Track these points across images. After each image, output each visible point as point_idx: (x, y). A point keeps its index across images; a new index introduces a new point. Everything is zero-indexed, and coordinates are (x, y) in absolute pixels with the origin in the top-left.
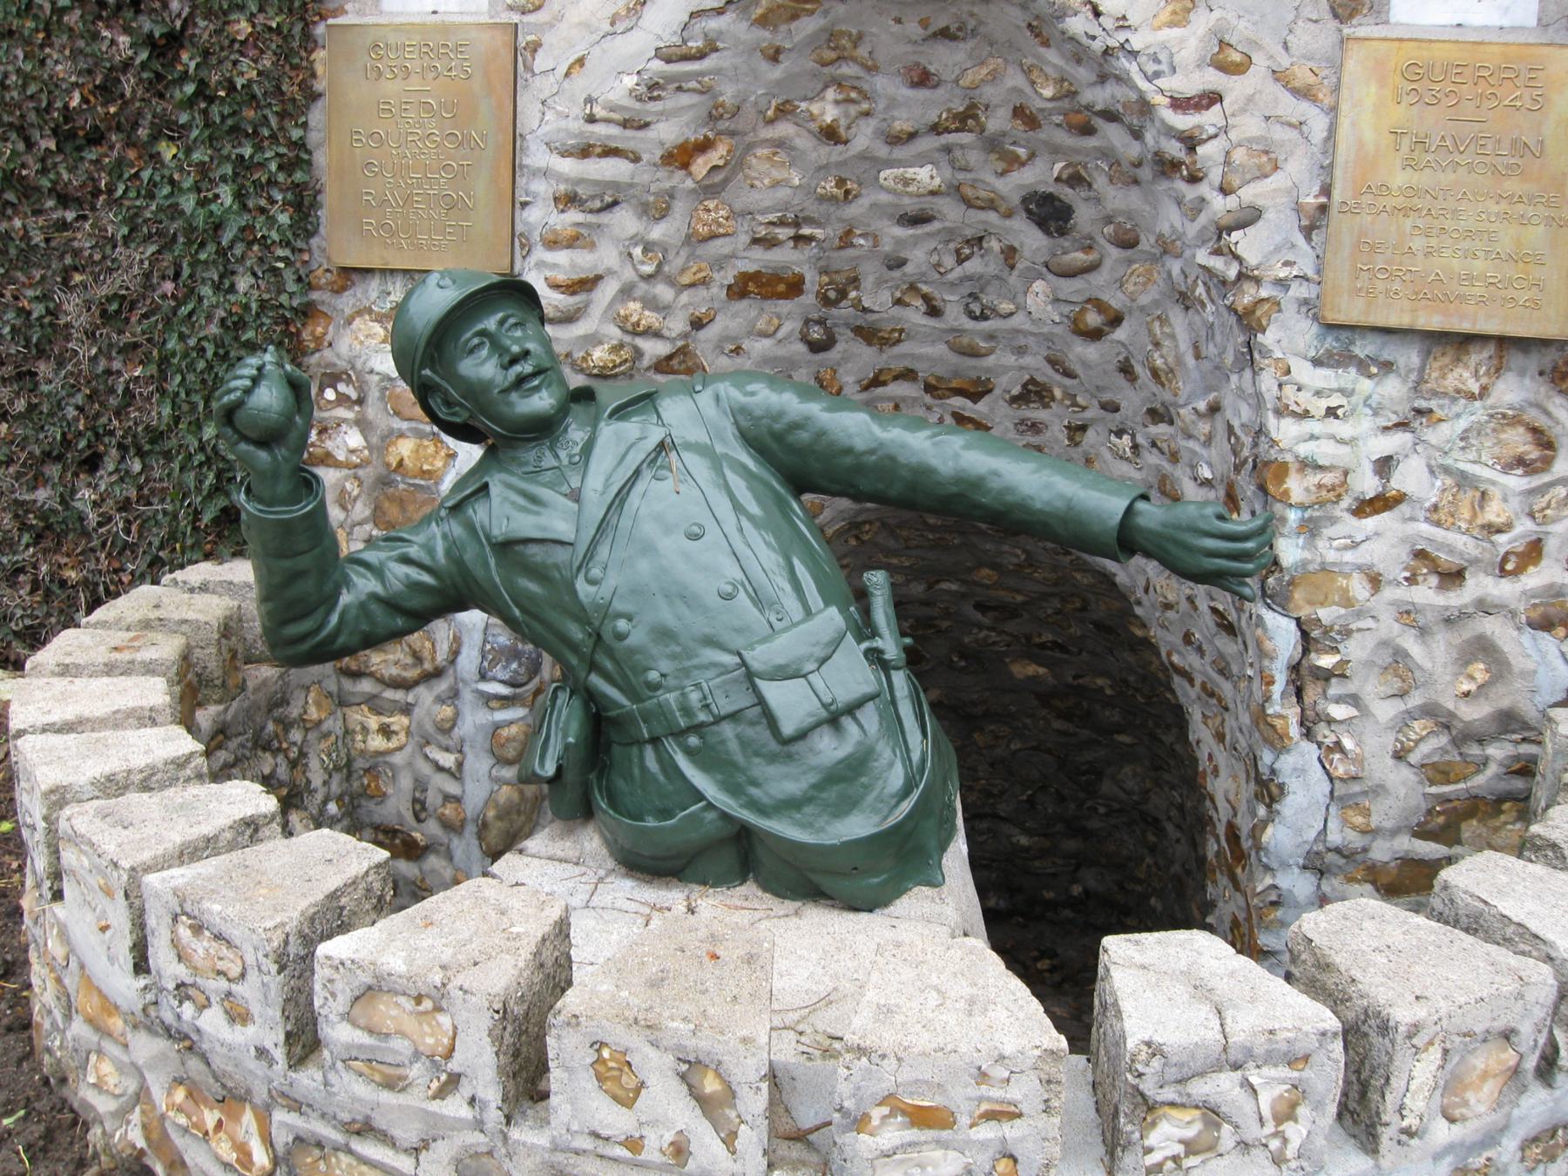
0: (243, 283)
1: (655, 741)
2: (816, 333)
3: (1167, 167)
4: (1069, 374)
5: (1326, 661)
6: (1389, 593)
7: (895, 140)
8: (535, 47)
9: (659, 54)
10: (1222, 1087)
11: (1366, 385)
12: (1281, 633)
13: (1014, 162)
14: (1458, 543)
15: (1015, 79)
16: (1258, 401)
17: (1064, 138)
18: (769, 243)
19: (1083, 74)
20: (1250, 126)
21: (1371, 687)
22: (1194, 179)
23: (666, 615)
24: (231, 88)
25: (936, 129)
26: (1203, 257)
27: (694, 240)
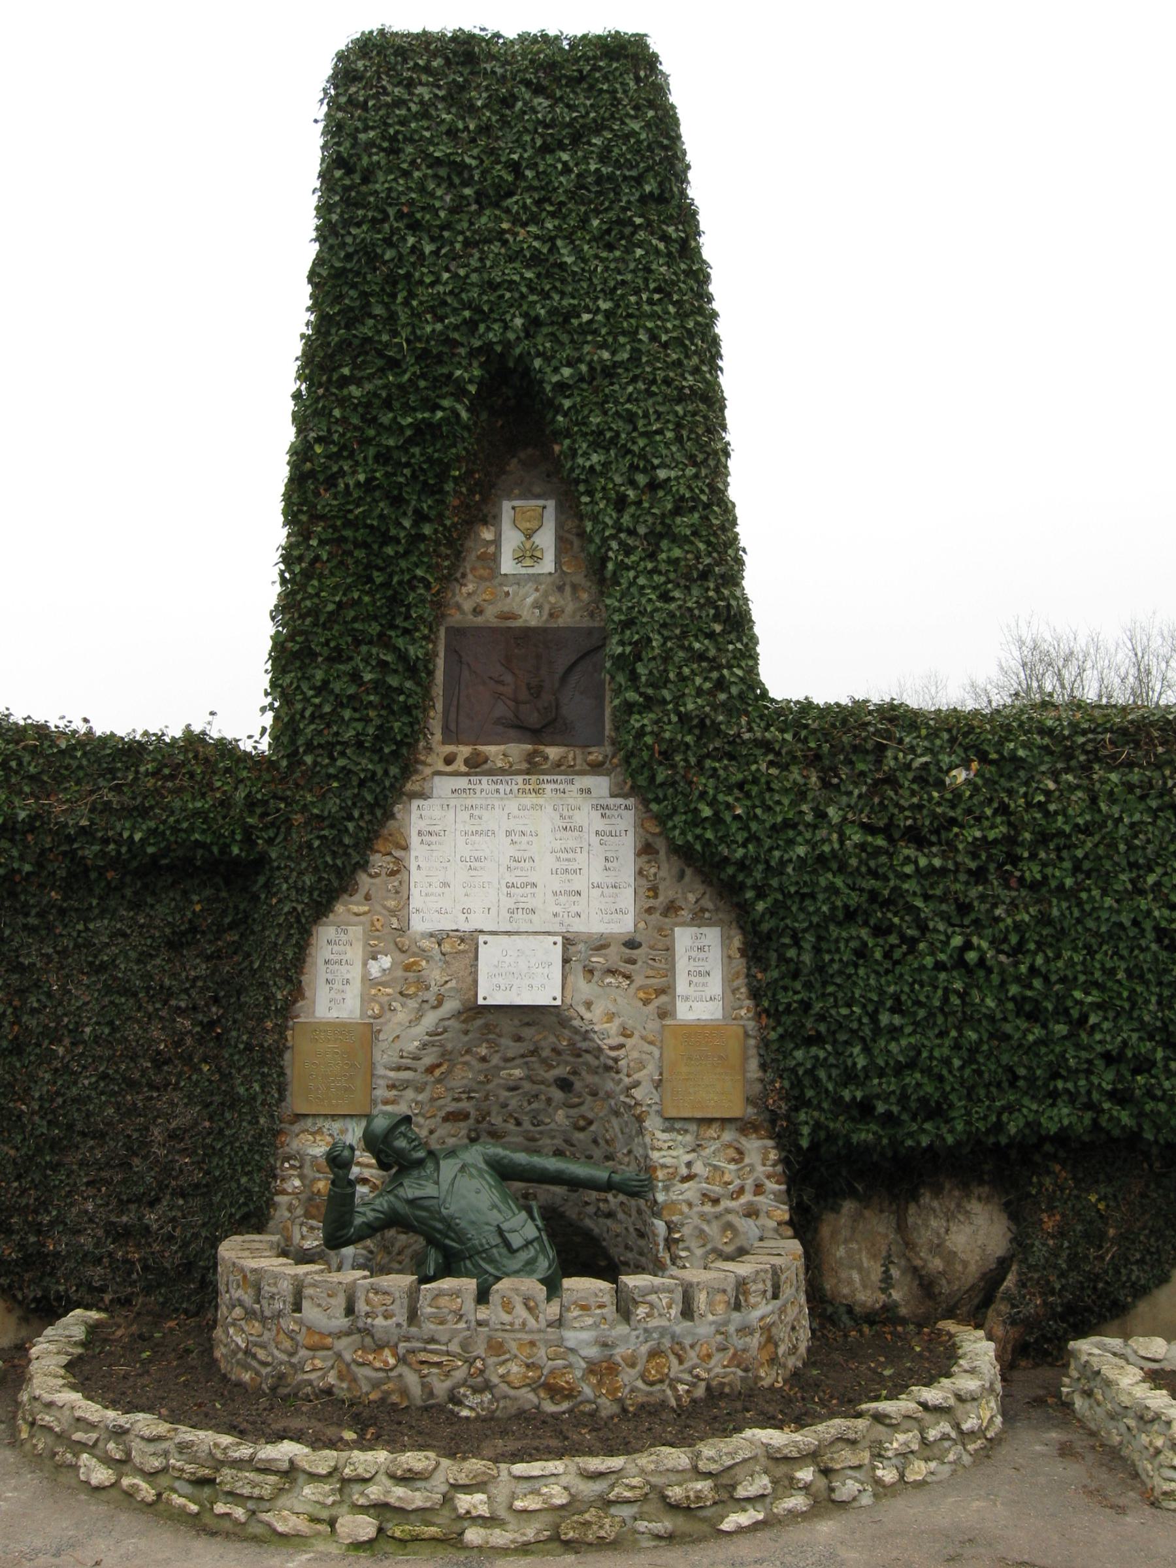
0: (262, 1120)
1: (470, 1257)
2: (473, 1135)
3: (608, 1068)
4: (572, 1145)
5: (677, 1236)
6: (695, 1209)
7: (507, 1060)
8: (379, 1031)
9: (427, 1034)
10: (653, 1298)
11: (680, 1138)
12: (660, 1226)
13: (551, 1067)
14: (717, 1189)
15: (552, 1039)
16: (645, 1146)
17: (571, 1059)
18: (458, 1100)
19: (577, 1038)
20: (635, 1055)
21: (693, 1244)
22: (618, 1072)
23: (473, 1217)
24: (262, 1046)
25: (523, 1056)
26: (622, 1098)
27: (433, 1100)
